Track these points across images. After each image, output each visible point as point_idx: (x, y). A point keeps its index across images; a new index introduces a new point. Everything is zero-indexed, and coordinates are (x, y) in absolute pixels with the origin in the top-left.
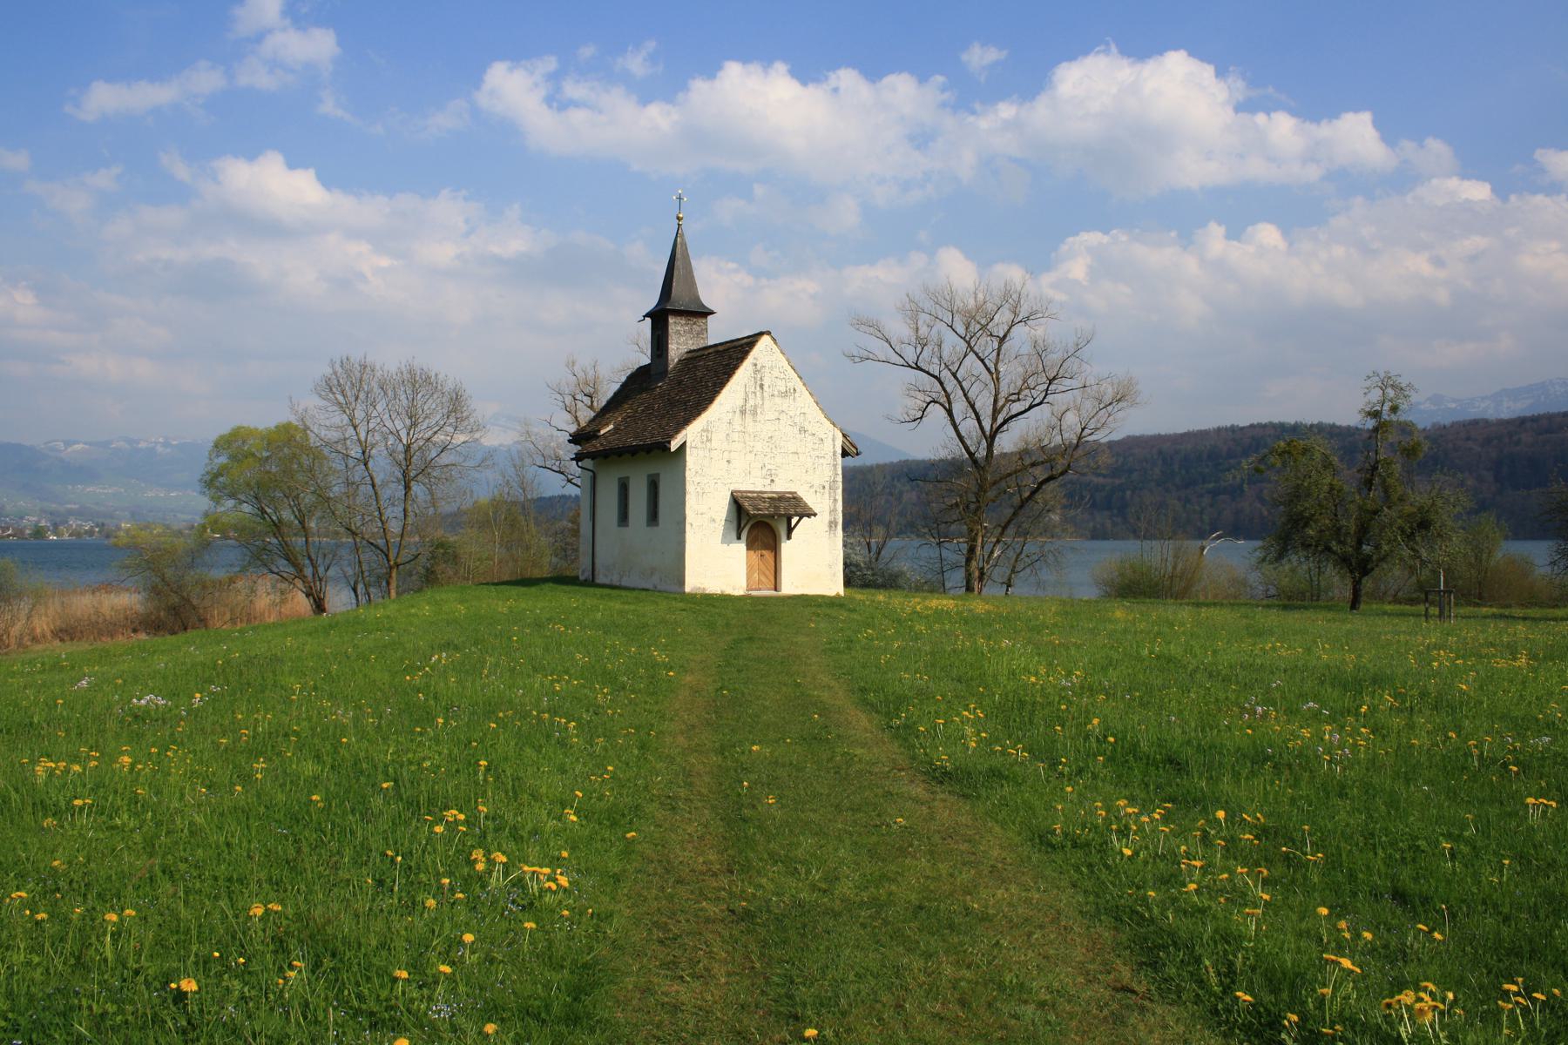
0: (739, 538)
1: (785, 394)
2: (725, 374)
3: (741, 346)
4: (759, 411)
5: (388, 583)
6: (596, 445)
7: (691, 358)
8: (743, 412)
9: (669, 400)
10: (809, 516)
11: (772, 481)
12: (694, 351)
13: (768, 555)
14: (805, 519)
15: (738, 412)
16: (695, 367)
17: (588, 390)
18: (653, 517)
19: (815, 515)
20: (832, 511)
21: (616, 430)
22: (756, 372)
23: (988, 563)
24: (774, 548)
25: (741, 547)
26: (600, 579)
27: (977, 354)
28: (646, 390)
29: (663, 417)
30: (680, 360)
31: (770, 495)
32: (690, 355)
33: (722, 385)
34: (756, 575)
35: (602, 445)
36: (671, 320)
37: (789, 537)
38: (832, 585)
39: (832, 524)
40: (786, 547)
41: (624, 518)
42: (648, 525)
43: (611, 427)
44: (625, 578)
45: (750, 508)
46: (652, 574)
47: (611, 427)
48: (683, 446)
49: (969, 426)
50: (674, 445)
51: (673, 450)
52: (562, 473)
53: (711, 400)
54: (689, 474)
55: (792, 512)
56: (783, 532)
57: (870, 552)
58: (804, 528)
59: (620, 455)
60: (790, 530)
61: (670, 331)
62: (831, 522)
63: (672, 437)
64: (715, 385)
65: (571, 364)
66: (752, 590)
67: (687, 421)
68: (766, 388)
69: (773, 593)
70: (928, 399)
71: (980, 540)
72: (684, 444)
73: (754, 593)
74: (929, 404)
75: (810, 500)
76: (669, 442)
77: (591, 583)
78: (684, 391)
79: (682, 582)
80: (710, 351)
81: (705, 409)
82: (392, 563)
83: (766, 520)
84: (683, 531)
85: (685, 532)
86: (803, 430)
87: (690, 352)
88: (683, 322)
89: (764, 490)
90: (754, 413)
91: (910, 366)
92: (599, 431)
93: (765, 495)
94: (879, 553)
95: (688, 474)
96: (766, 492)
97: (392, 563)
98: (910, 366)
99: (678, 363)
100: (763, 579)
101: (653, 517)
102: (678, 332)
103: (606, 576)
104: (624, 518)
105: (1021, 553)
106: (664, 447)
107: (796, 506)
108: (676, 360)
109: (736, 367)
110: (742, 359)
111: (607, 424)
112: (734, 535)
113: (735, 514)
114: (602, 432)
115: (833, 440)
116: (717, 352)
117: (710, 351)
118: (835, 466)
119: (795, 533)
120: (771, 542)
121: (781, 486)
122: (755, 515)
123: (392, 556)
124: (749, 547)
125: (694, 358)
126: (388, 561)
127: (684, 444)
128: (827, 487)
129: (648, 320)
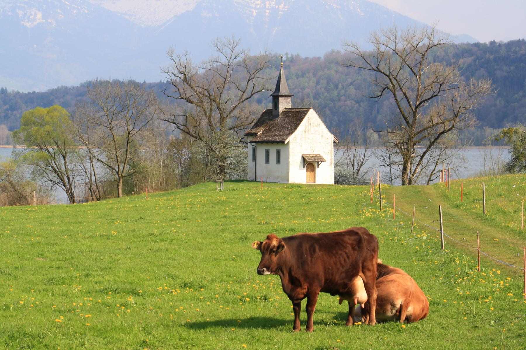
0: (304, 168)
1: (317, 126)
2: (299, 120)
3: (304, 111)
4: (309, 131)
5: (118, 186)
6: (257, 139)
7: (287, 111)
8: (305, 132)
9: (281, 126)
10: (324, 161)
11: (313, 151)
12: (287, 109)
13: (312, 173)
14: (323, 162)
15: (304, 132)
16: (289, 115)
17: (182, 69)
18: (278, 161)
19: (326, 161)
20: (331, 159)
21: (263, 133)
22: (308, 120)
23: (413, 175)
24: (313, 170)
25: (304, 171)
26: (258, 180)
27: (408, 65)
28: (271, 120)
29: (280, 132)
30: (283, 111)
31: (313, 155)
32: (286, 110)
33: (299, 124)
34: (309, 178)
35: (260, 139)
36: (280, 98)
37: (318, 167)
38: (331, 181)
39: (331, 163)
40: (317, 170)
41: (267, 161)
42: (276, 164)
43: (261, 132)
44: (268, 180)
45: (307, 160)
46: (278, 178)
47: (261, 132)
48: (289, 142)
49: (404, 104)
50: (286, 142)
51: (286, 143)
52: (175, 123)
53: (296, 129)
54: (290, 150)
55: (319, 160)
56: (316, 165)
57: (353, 169)
58: (322, 165)
59: (267, 143)
60: (318, 165)
61: (280, 102)
62: (330, 163)
63: (285, 139)
64: (297, 123)
65: (170, 53)
66: (308, 183)
67: (289, 135)
68: (311, 124)
69: (314, 184)
70: (385, 87)
71: (409, 164)
72: (289, 141)
73: (308, 184)
74: (385, 89)
75: (324, 157)
76: (285, 141)
77: (255, 180)
78: (286, 123)
79: (288, 180)
80: (294, 110)
81: (294, 131)
82: (120, 176)
83: (312, 163)
84: (288, 166)
85: (289, 166)
86: (322, 136)
87: (286, 109)
88: (284, 99)
89: (311, 154)
90: (308, 132)
91: (374, 70)
92: (257, 134)
93: (311, 156)
94: (359, 170)
95: (290, 150)
96: (311, 155)
97: (120, 176)
98: (374, 70)
99: (282, 112)
100: (311, 179)
101: (278, 161)
102: (282, 102)
103: (261, 179)
104: (267, 161)
105: (434, 170)
106: (283, 142)
107: (320, 159)
108: (282, 111)
109: (303, 119)
110: (305, 116)
111: (259, 131)
112: (303, 167)
113: (303, 161)
114: (258, 134)
115: (331, 139)
116: (296, 111)
117: (294, 110)
118: (332, 146)
119: (320, 166)
120: (313, 169)
121: (316, 153)
122: (309, 162)
123: (120, 173)
124: (307, 171)
125: (287, 112)
126: (353, 169)
127: (289, 141)
128: (329, 153)
129: (272, 97)
